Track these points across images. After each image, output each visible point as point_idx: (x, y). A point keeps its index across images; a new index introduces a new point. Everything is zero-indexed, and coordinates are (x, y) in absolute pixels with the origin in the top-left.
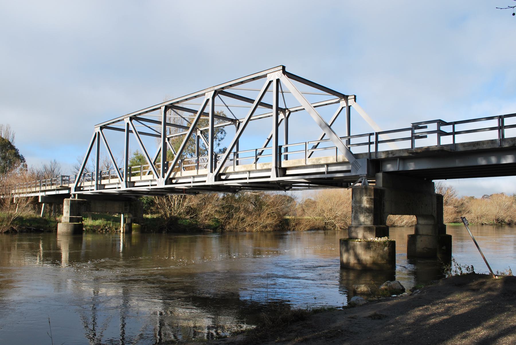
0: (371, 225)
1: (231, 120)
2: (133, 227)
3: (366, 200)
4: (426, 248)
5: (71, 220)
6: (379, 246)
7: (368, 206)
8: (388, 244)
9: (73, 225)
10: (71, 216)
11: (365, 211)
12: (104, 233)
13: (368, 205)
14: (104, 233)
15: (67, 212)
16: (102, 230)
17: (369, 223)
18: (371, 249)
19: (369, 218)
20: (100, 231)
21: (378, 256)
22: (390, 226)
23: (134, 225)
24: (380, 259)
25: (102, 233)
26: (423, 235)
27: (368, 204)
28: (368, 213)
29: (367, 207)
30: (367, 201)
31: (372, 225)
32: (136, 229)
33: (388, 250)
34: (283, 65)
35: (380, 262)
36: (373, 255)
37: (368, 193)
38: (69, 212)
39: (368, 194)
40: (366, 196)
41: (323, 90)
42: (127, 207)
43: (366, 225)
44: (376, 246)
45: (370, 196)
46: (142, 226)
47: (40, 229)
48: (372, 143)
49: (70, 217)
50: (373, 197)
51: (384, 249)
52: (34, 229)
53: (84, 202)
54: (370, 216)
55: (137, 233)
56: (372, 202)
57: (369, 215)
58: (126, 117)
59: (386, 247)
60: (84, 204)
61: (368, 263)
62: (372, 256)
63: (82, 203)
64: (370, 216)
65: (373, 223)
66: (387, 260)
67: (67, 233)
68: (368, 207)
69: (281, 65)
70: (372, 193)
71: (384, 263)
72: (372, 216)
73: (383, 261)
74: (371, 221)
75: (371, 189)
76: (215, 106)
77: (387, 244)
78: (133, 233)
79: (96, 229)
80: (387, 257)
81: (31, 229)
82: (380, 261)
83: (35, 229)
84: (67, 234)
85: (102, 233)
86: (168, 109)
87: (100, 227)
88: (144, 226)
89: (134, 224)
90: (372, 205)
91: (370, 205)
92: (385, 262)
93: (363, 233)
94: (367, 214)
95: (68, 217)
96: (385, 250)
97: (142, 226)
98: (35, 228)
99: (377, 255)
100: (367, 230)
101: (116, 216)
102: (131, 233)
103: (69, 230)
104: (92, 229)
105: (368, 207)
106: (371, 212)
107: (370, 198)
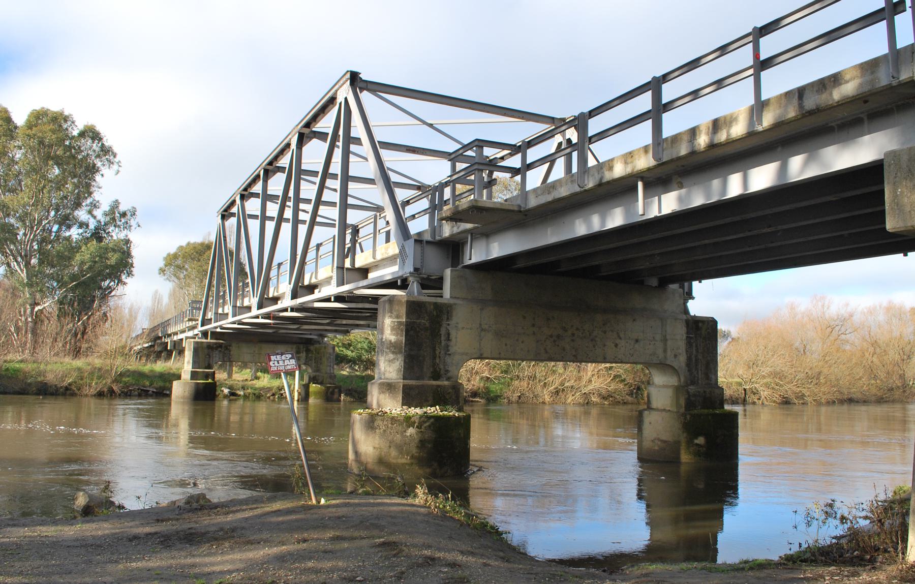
0: (398, 379)
1: (416, 187)
2: (311, 389)
3: (390, 326)
4: (659, 439)
5: (194, 375)
6: (393, 425)
7: (393, 338)
8: (417, 421)
9: (193, 385)
10: (194, 370)
11: (387, 349)
12: (277, 400)
13: (394, 337)
14: (277, 400)
15: (188, 362)
16: (273, 395)
17: (394, 375)
18: (376, 432)
19: (394, 365)
20: (269, 398)
21: (390, 447)
22: (873, 398)
23: (314, 387)
24: (394, 453)
25: (274, 401)
26: (657, 410)
27: (394, 335)
28: (393, 353)
29: (390, 341)
30: (393, 329)
31: (401, 379)
32: (317, 394)
33: (417, 434)
34: (351, 70)
35: (395, 461)
36: (379, 444)
37: (393, 311)
38: (191, 362)
39: (395, 313)
40: (391, 317)
41: (505, 115)
42: (302, 354)
43: (387, 379)
44: (386, 425)
45: (397, 317)
46: (328, 388)
47: (165, 392)
48: (273, 198)
49: (192, 372)
50: (404, 320)
51: (405, 431)
52: (153, 392)
53: (220, 346)
54: (397, 360)
55: (319, 401)
56: (402, 331)
57: (394, 359)
58: (235, 195)
59: (411, 428)
60: (220, 349)
61: (370, 460)
62: (377, 446)
63: (215, 346)
64: (397, 360)
65: (403, 376)
66: (412, 457)
67: (183, 397)
68: (393, 341)
69: (348, 71)
70: (403, 310)
71: (407, 464)
72: (400, 360)
73: (401, 458)
74: (399, 370)
75: (400, 302)
76: (350, 163)
77: (415, 422)
78: (311, 400)
79: (263, 394)
80: (414, 451)
81: (149, 391)
82: (394, 456)
83: (155, 390)
84: (182, 400)
85: (274, 401)
86: (270, 174)
87: (272, 390)
88: (331, 390)
89: (314, 385)
90: (402, 336)
91: (397, 336)
92: (408, 462)
93: (378, 397)
94: (391, 356)
95: (188, 371)
96: (408, 434)
97: (328, 388)
98: (156, 389)
99: (388, 445)
100: (384, 390)
101: (345, 373)
102: (308, 400)
103: (187, 394)
104: (255, 394)
105: (393, 341)
106: (400, 352)
107: (398, 322)
